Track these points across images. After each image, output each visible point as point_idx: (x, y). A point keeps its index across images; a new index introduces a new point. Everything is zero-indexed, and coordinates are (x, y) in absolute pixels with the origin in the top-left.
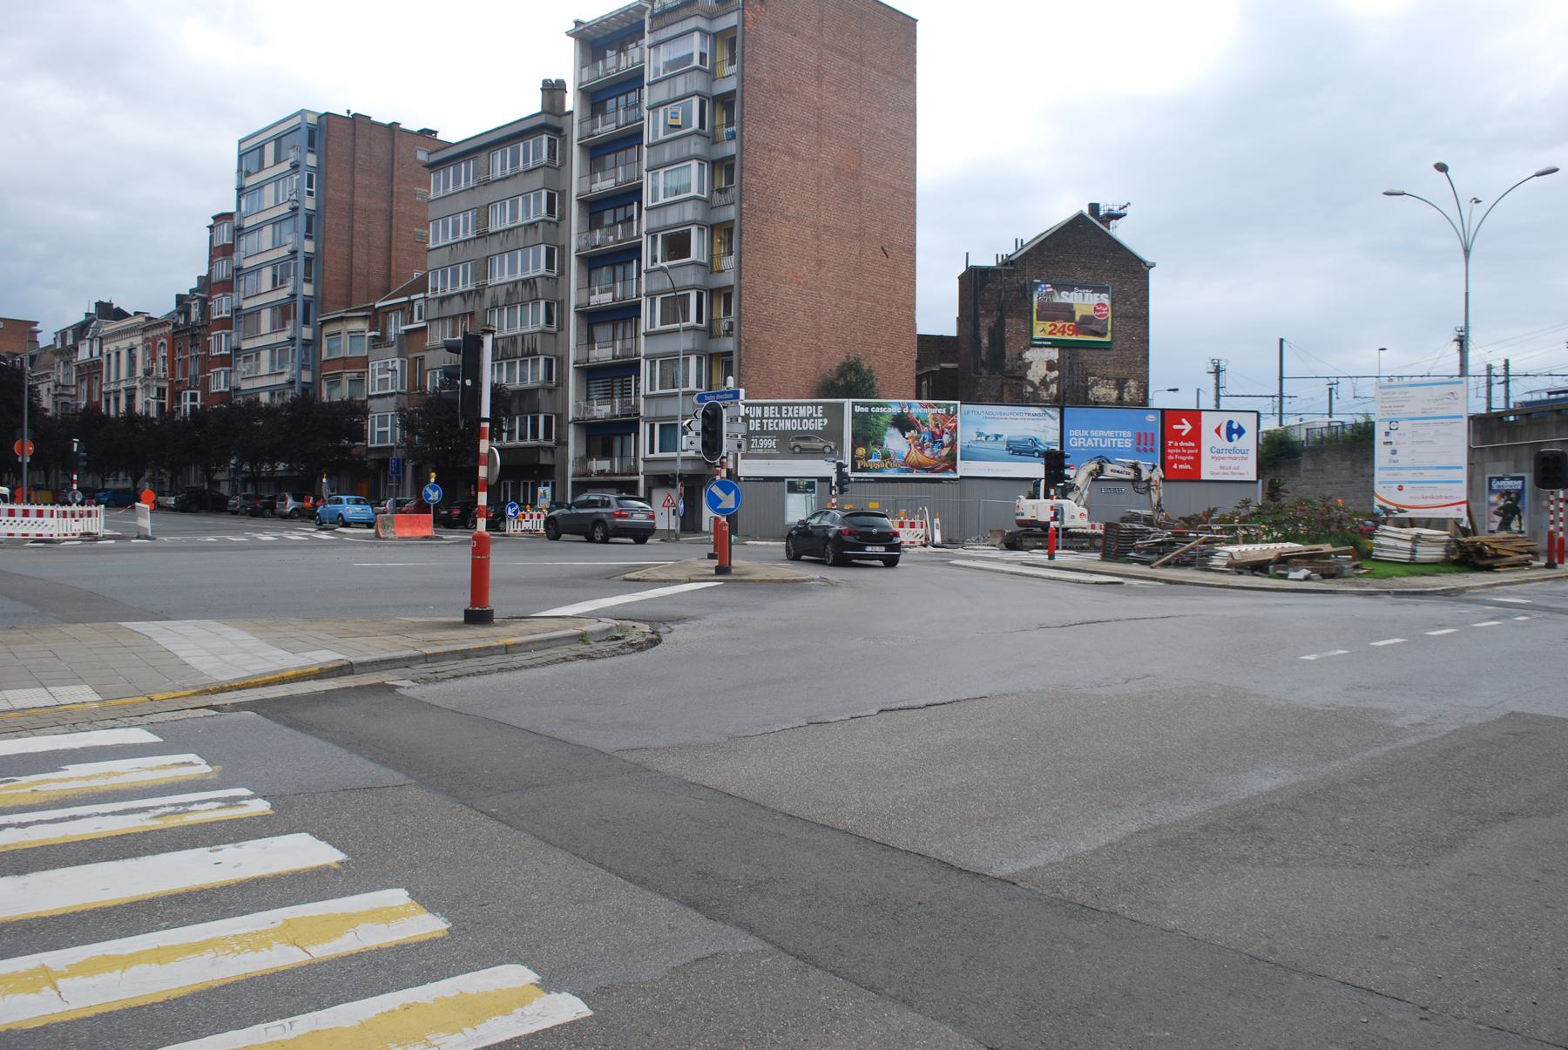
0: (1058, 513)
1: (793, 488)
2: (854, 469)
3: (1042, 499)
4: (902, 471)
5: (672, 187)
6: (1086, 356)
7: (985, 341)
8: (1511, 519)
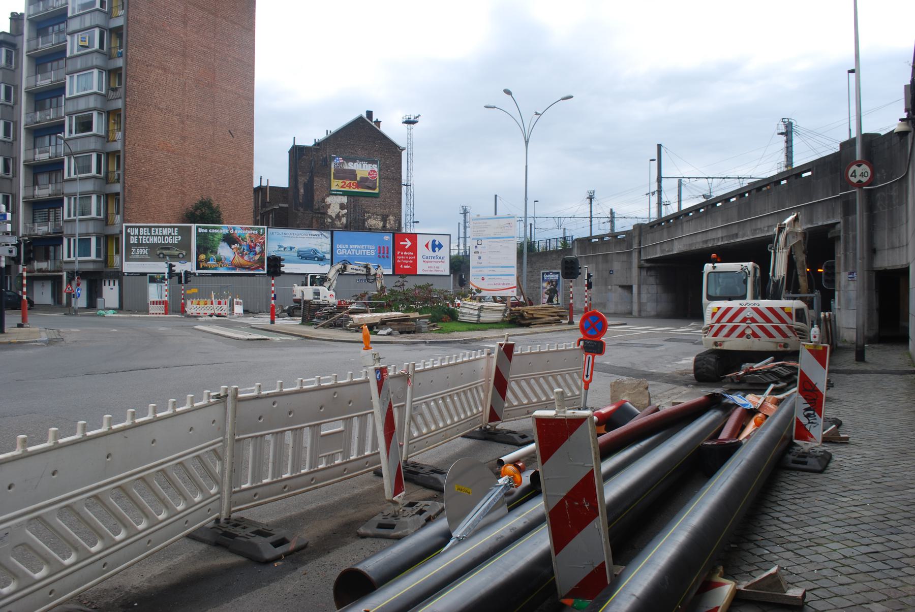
0: (317, 294)
1: (153, 280)
3: (309, 286)
4: (229, 269)
5: (83, 86)
6: (364, 201)
7: (302, 191)
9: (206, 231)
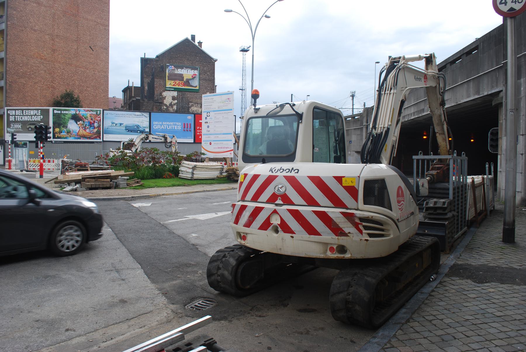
2: (54, 137)
4: (76, 138)
6: (188, 95)
8: (191, 158)
9: (59, 112)
